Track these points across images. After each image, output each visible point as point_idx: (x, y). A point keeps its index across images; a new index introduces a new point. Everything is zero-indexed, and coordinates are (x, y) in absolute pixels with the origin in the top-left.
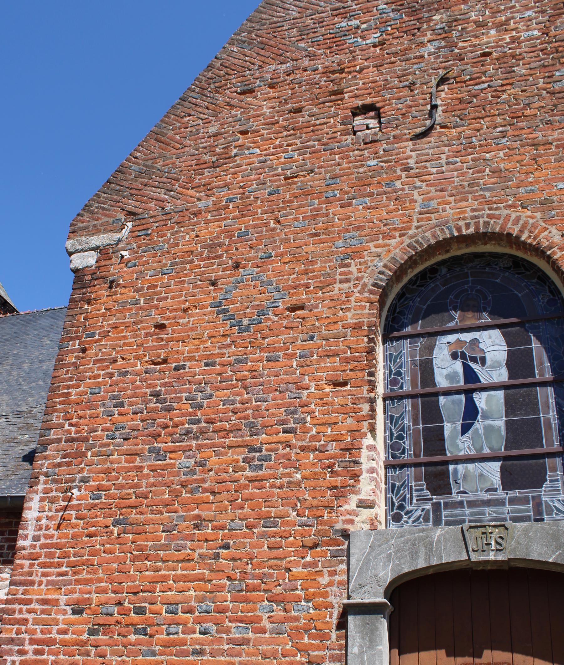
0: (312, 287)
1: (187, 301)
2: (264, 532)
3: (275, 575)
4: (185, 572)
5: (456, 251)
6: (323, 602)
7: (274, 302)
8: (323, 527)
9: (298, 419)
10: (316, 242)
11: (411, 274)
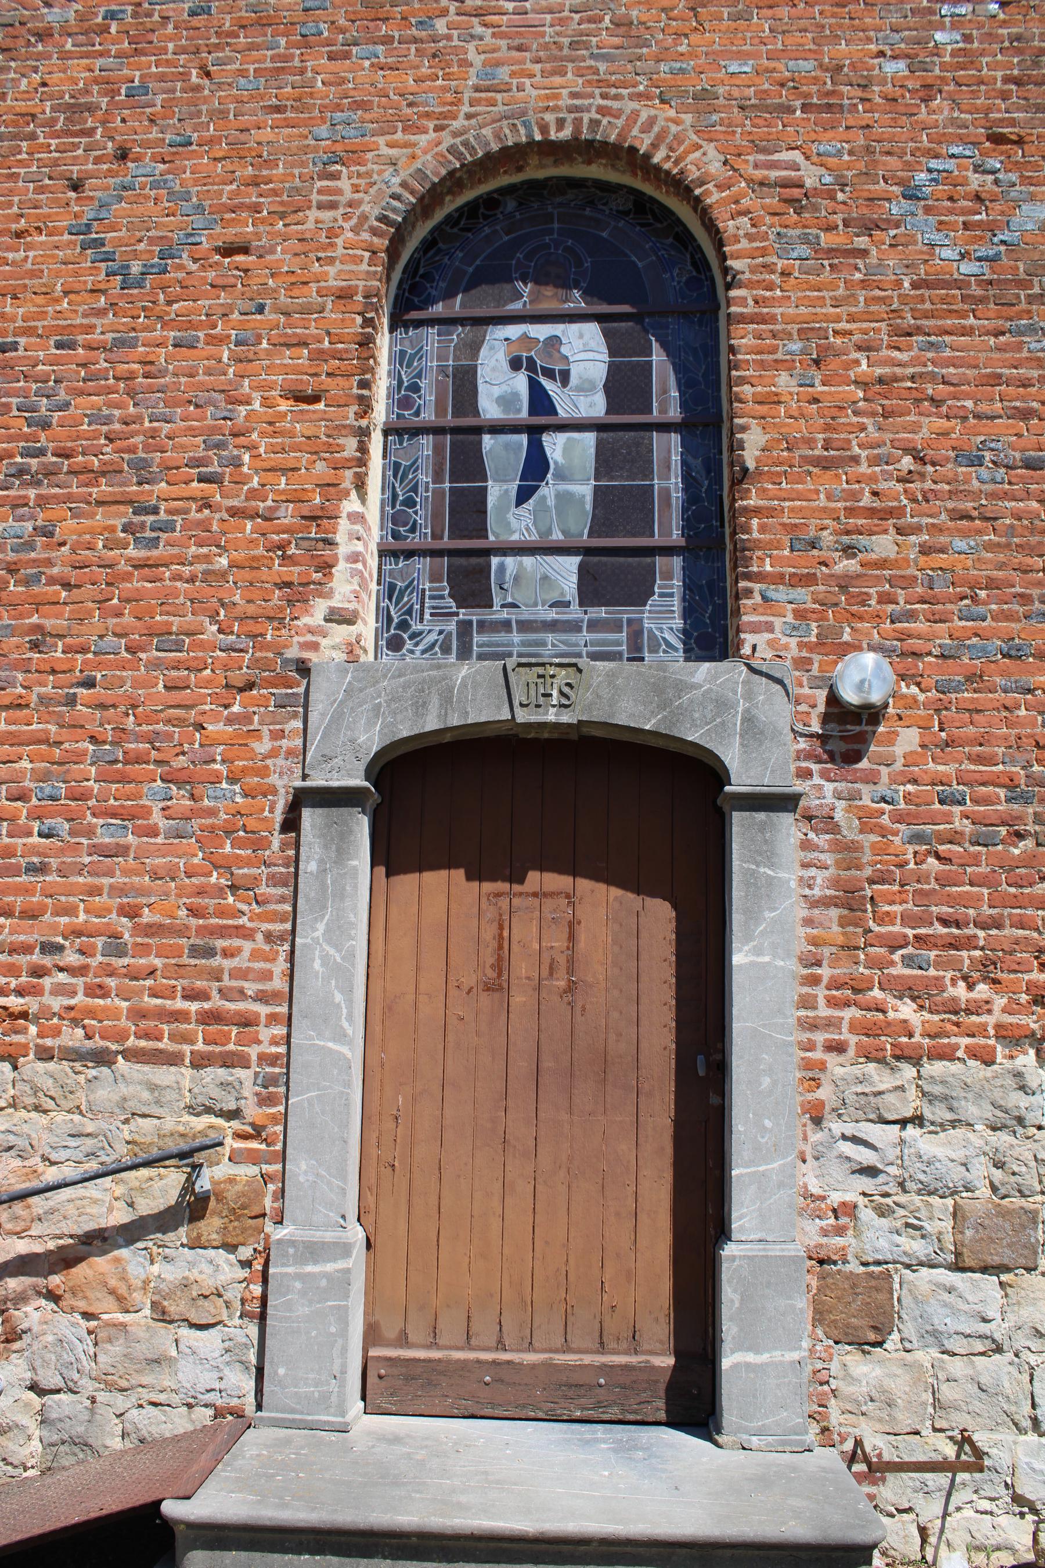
0: (265, 212)
1: (22, 216)
2: (158, 658)
3: (176, 736)
4: (13, 728)
5: (536, 171)
6: (259, 784)
7: (192, 235)
8: (264, 654)
9: (226, 458)
10: (278, 123)
11: (451, 205)
